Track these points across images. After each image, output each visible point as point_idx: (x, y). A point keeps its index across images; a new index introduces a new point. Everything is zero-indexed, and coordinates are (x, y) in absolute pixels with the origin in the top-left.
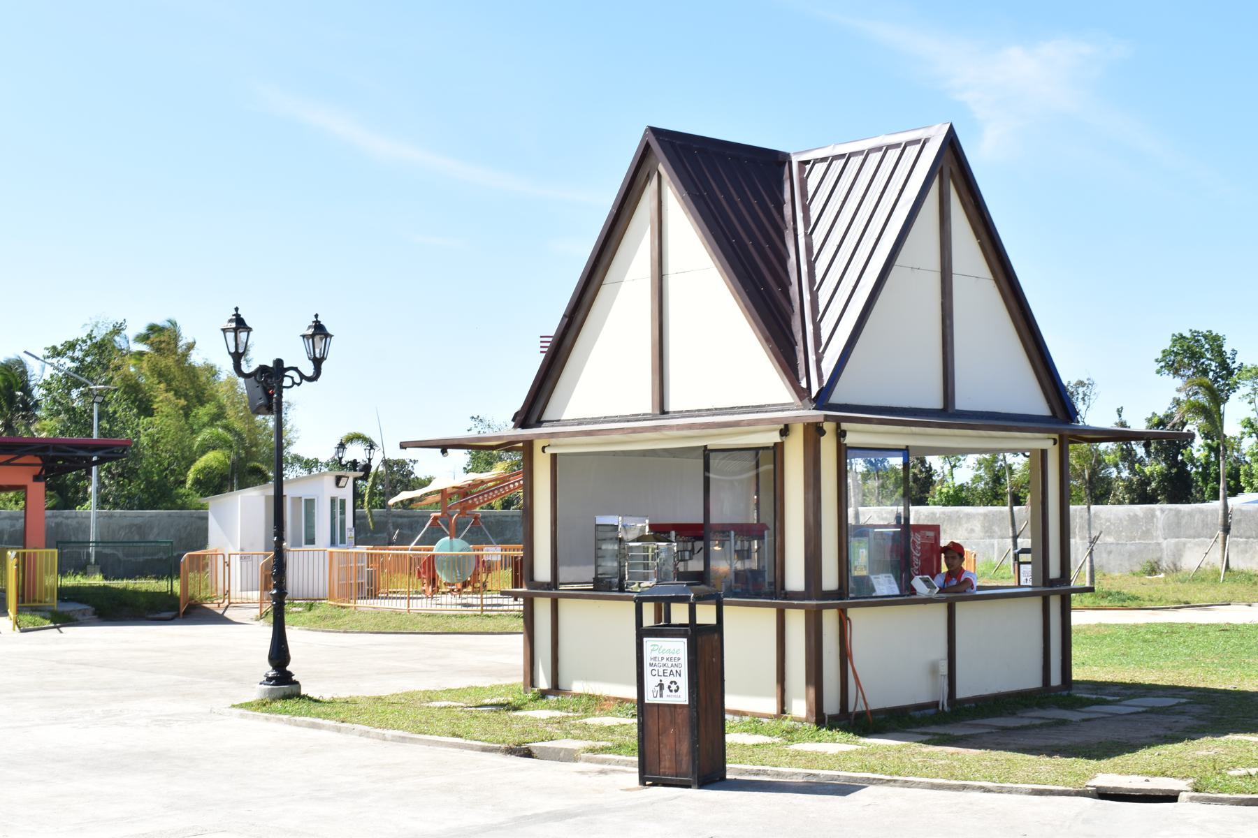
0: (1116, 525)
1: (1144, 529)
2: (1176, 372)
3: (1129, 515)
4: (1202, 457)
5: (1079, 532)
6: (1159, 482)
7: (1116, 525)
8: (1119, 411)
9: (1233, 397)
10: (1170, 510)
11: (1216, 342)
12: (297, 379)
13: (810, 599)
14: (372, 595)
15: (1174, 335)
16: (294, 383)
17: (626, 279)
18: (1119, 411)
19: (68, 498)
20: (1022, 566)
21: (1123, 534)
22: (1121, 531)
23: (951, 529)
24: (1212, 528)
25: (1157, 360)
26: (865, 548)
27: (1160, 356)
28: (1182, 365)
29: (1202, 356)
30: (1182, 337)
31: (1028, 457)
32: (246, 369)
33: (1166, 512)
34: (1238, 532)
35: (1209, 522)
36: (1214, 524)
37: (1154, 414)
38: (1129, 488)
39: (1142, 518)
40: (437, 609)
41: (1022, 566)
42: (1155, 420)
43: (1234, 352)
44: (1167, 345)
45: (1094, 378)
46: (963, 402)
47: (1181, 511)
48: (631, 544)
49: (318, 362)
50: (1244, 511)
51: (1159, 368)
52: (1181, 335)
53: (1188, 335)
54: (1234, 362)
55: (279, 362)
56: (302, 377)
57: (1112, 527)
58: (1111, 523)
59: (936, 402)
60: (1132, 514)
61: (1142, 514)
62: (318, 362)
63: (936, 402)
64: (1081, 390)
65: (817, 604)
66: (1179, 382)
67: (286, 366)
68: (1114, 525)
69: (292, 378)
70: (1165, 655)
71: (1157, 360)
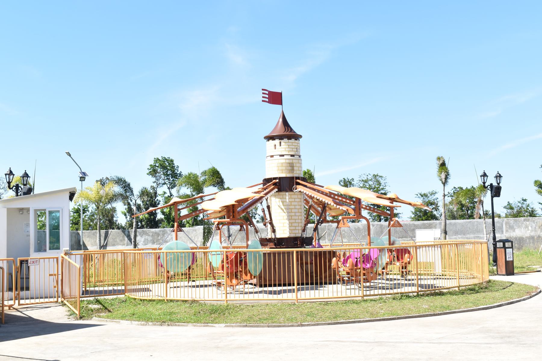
0: (348, 233)
1: (363, 234)
3: (355, 228)
4: (167, 211)
5: (327, 237)
6: (146, 222)
7: (348, 233)
10: (377, 225)
13: (329, 280)
14: (330, 280)
15: (155, 158)
20: (507, 250)
21: (352, 237)
22: (351, 236)
23: (252, 237)
24: (400, 234)
25: (148, 169)
26: (251, 244)
31: (487, 186)
33: (375, 226)
34: (413, 235)
35: (398, 230)
36: (401, 231)
38: (173, 223)
39: (362, 229)
40: (269, 299)
41: (507, 250)
47: (383, 225)
48: (105, 244)
50: (416, 225)
51: (148, 172)
52: (158, 159)
53: (161, 159)
54: (178, 171)
57: (346, 234)
58: (345, 232)
60: (356, 227)
61: (362, 227)
65: (267, 285)
68: (347, 233)
70: (135, 317)
71: (148, 169)
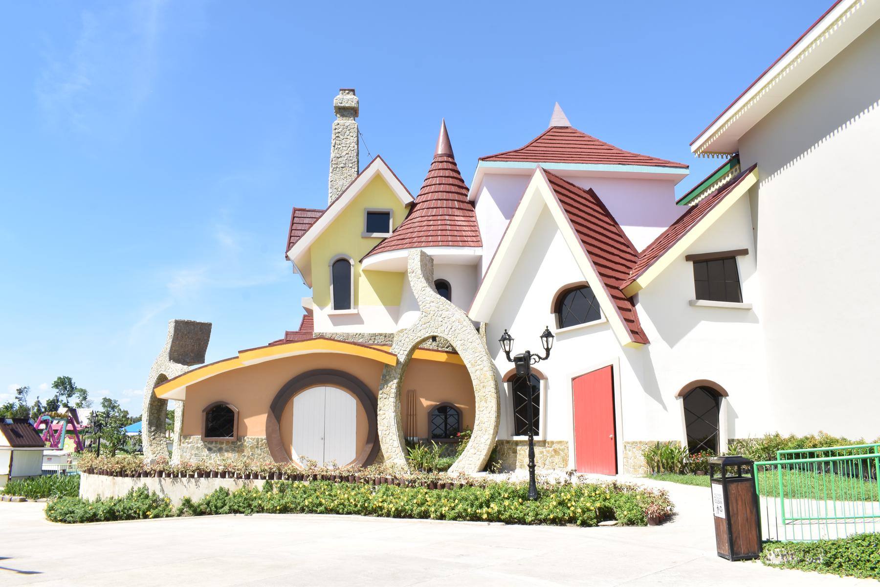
2: (57, 388)
8: (38, 398)
9: (73, 396)
11: (70, 380)
12: (537, 359)
16: (536, 362)
17: (585, 280)
18: (38, 398)
19: (206, 504)
27: (53, 383)
28: (60, 386)
29: (65, 384)
30: (60, 378)
32: (433, 432)
37: (49, 400)
42: (50, 401)
43: (74, 383)
44: (56, 380)
45: (30, 386)
46: (721, 261)
49: (548, 350)
53: (62, 377)
55: (528, 352)
56: (540, 358)
59: (708, 263)
62: (548, 350)
63: (725, 261)
64: (25, 390)
66: (57, 390)
67: (531, 353)
69: (535, 359)
